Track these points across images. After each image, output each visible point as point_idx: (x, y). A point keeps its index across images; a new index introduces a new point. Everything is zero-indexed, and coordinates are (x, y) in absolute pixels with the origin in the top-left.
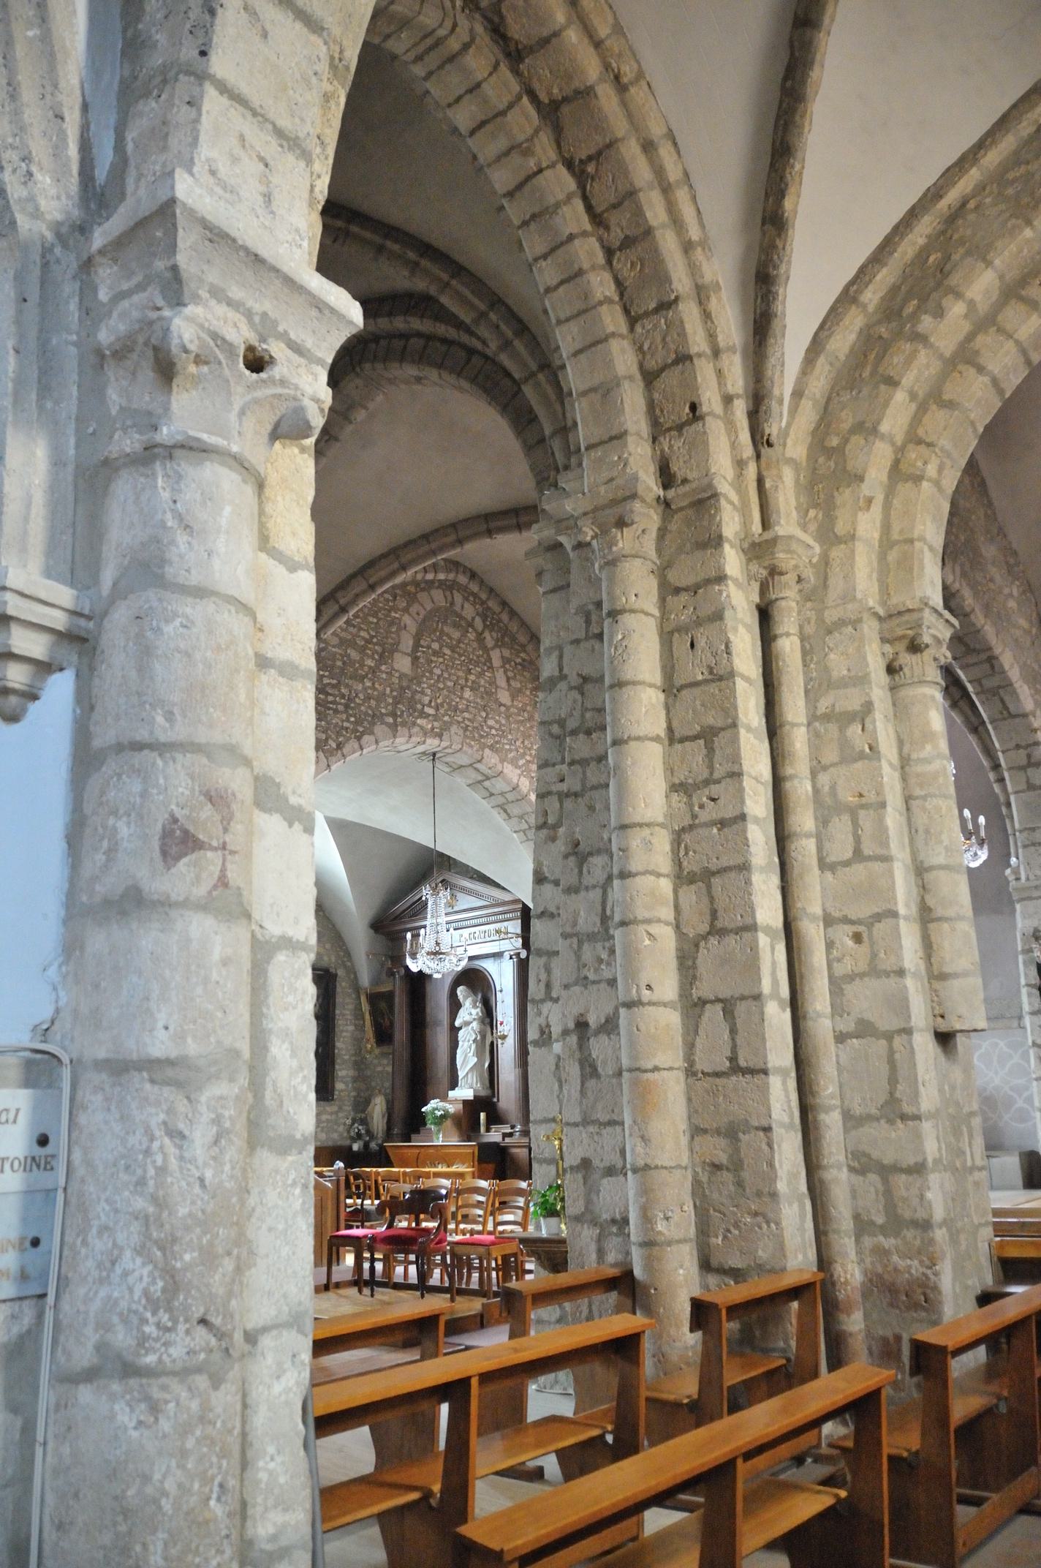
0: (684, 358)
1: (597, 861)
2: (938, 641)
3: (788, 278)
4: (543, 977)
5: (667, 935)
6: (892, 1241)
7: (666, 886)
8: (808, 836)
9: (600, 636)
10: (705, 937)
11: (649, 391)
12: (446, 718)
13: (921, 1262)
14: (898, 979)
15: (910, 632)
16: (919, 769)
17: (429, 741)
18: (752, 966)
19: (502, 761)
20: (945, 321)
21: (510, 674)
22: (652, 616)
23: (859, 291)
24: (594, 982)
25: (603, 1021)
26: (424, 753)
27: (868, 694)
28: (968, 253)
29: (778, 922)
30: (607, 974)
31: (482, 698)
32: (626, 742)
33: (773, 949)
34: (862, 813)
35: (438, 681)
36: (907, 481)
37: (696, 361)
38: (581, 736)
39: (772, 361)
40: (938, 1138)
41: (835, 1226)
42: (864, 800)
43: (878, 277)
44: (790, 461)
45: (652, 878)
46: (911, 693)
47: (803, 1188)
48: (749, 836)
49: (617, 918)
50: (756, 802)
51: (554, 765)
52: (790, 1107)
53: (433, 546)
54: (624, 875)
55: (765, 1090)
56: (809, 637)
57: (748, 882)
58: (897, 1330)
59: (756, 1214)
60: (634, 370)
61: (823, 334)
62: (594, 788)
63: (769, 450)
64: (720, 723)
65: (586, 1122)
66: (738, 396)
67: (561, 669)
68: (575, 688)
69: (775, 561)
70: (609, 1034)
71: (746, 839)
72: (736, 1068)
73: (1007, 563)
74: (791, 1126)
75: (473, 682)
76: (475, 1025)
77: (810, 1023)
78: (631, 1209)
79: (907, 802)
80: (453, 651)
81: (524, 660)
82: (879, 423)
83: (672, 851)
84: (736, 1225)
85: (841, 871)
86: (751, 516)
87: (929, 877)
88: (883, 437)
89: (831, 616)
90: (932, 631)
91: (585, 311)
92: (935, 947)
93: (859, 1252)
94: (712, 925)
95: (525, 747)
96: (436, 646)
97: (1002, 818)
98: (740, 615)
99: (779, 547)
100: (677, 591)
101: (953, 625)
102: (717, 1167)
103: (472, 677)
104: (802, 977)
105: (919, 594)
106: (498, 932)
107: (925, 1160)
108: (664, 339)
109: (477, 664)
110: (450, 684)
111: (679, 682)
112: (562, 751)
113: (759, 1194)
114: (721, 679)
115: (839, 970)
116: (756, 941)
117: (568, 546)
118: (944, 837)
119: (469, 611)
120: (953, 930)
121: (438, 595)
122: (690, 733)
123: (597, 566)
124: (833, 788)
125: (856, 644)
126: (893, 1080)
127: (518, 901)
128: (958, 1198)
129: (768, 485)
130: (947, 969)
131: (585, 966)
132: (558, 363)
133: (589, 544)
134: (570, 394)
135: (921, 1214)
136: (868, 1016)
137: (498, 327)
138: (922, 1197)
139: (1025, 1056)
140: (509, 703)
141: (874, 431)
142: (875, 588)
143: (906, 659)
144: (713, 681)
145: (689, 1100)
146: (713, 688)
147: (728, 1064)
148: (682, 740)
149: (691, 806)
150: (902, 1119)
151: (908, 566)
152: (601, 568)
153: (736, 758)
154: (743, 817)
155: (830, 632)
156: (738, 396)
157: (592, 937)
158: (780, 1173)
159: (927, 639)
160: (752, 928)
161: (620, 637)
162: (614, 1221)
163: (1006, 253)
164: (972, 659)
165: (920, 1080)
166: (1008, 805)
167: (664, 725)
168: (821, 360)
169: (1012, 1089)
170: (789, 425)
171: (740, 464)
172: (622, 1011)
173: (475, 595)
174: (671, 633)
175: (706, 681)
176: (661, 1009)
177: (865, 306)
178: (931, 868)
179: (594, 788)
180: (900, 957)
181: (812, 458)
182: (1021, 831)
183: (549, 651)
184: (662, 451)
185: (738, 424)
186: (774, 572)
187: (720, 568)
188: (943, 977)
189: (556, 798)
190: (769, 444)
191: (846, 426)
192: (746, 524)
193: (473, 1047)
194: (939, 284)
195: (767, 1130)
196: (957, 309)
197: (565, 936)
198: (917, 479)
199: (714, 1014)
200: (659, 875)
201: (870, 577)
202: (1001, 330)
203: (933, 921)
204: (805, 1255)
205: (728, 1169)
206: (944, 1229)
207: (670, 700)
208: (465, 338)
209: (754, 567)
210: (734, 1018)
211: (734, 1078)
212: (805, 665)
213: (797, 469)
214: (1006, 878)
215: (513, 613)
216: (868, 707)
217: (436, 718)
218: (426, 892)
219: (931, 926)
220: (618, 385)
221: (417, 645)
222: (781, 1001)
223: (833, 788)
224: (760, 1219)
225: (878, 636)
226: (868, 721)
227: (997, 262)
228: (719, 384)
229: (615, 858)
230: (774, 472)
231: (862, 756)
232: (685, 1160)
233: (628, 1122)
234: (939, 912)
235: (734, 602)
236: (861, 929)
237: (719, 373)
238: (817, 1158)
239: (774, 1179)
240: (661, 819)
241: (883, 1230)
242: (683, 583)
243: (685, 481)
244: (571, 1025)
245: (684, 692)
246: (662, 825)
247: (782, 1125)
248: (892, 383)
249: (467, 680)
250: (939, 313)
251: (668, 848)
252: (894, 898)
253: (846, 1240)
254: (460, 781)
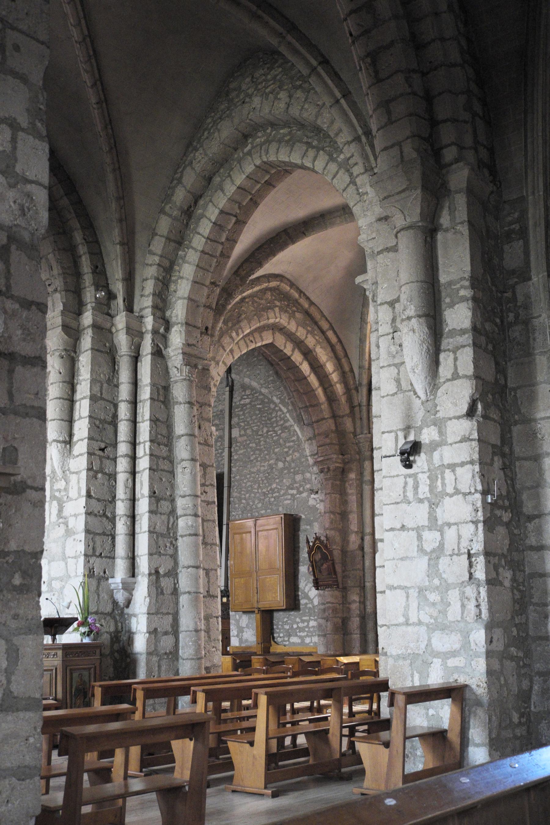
24: (163, 555)
162: (166, 653)
244: (153, 571)
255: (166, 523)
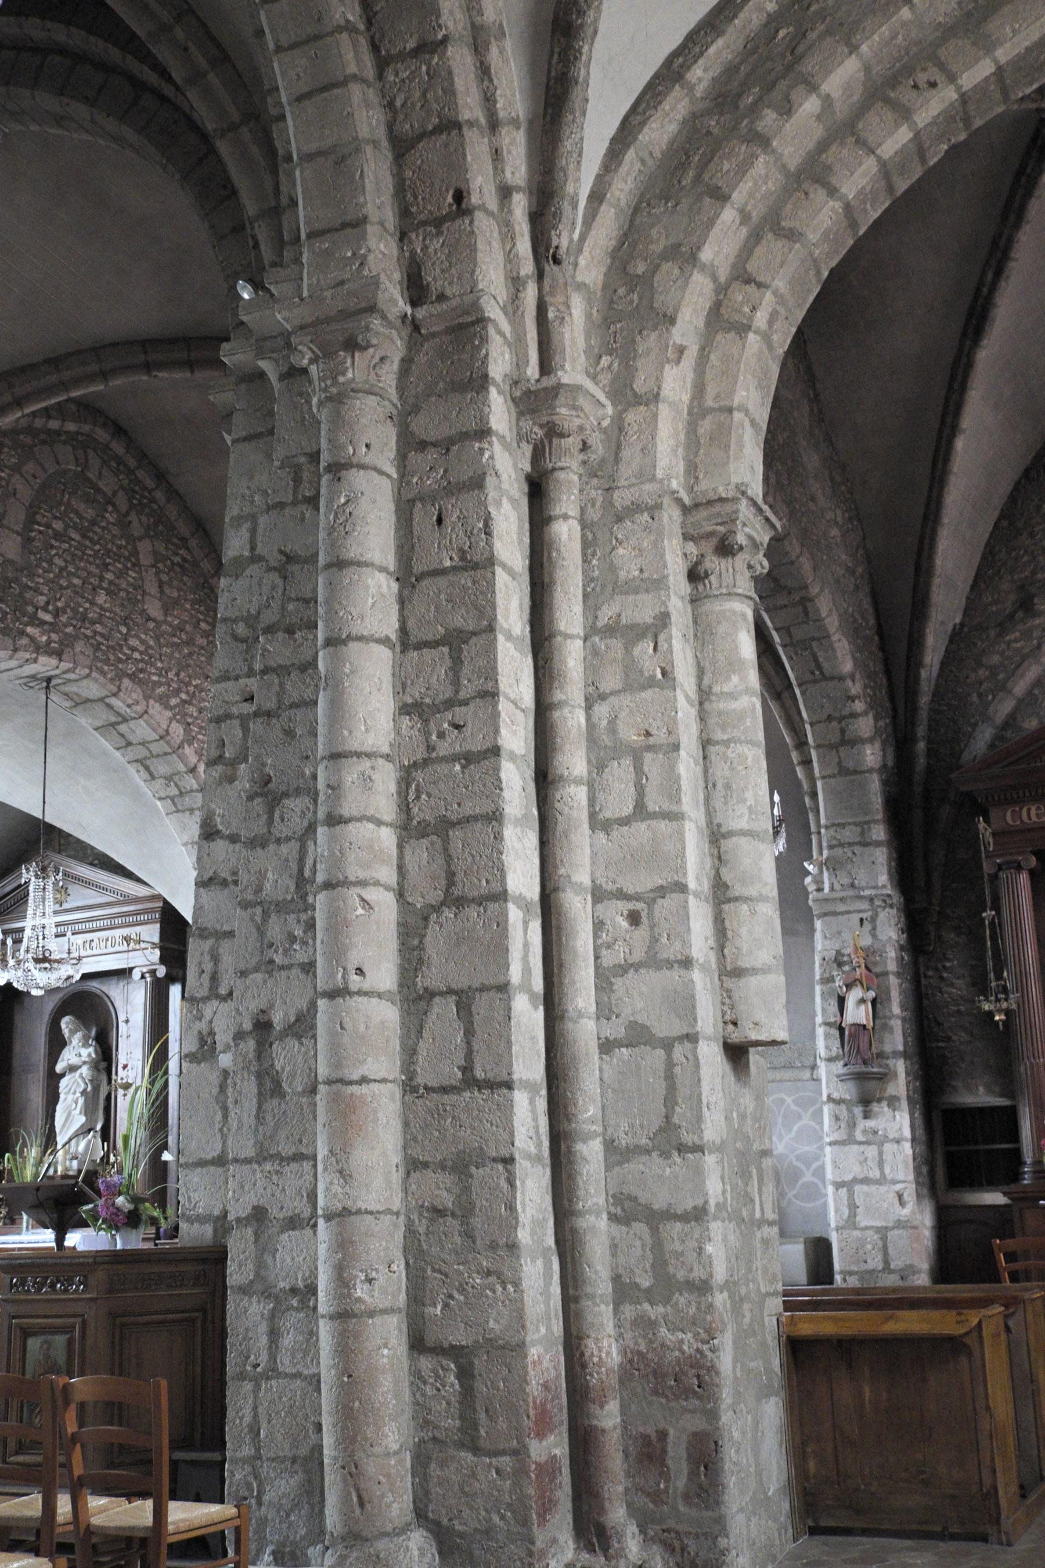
0: (451, 126)
1: (295, 805)
2: (755, 545)
3: (596, 32)
4: (208, 967)
5: (385, 903)
6: (661, 1309)
7: (388, 838)
8: (578, 782)
9: (313, 501)
10: (437, 909)
11: (400, 166)
12: (69, 630)
13: (696, 1335)
14: (683, 972)
15: (721, 529)
16: (722, 705)
17: (43, 659)
18: (499, 948)
19: (147, 698)
20: (793, 120)
21: (165, 578)
22: (388, 476)
23: (687, 67)
24: (282, 968)
25: (292, 1019)
26: (33, 677)
27: (664, 603)
28: (828, 32)
29: (533, 893)
30: (301, 955)
31: (122, 605)
32: (344, 642)
33: (526, 924)
34: (648, 757)
35: (59, 576)
36: (729, 331)
37: (465, 129)
38: (280, 635)
39: (568, 145)
40: (722, 1178)
41: (589, 1290)
42: (651, 741)
43: (712, 50)
44: (581, 287)
45: (371, 826)
46: (717, 607)
47: (550, 1241)
48: (503, 775)
49: (320, 878)
50: (515, 733)
51: (237, 678)
52: (537, 1132)
53: (66, 375)
54: (335, 820)
55: (508, 1107)
56: (593, 524)
57: (498, 837)
58: (662, 1425)
59: (489, 1273)
60: (381, 133)
61: (636, 120)
62: (294, 706)
63: (555, 268)
64: (471, 627)
65: (262, 1157)
66: (518, 189)
67: (253, 549)
68: (275, 569)
69: (555, 418)
70: (299, 1037)
71: (499, 780)
72: (470, 1081)
73: (832, 479)
74: (538, 1158)
75: (111, 583)
76: (85, 1070)
77: (570, 1025)
78: (321, 1269)
79: (704, 748)
80: (84, 536)
81: (184, 560)
82: (699, 248)
83: (399, 793)
84: (462, 1290)
85: (616, 832)
86: (526, 355)
87: (727, 844)
88: (703, 268)
89: (622, 498)
90: (747, 530)
91: (317, 37)
92: (730, 934)
93: (618, 1326)
94: (447, 892)
95: (180, 681)
96: (58, 525)
97: (803, 812)
98: (505, 486)
99: (561, 399)
100: (423, 445)
101: (773, 526)
102: (438, 1212)
103: (109, 576)
104: (561, 966)
105: (735, 479)
106: (127, 939)
107: (706, 1202)
108: (424, 94)
109: (118, 557)
110: (76, 581)
111: (418, 568)
112: (248, 661)
113: (493, 1246)
114: (475, 566)
115: (609, 959)
116: (505, 914)
117: (273, 377)
118: (749, 795)
119: (108, 484)
120: (753, 913)
121: (65, 452)
122: (430, 637)
123: (315, 401)
124: (613, 722)
125: (653, 538)
126: (670, 1100)
127: (158, 897)
128: (743, 1256)
129: (551, 315)
130: (745, 963)
131: (271, 945)
132: (274, 112)
133: (304, 371)
134: (289, 158)
135: (698, 1273)
136: (641, 1019)
137: (186, 49)
138: (700, 1250)
139: (818, 1115)
140: (161, 618)
141: (692, 258)
142: (681, 467)
143: (712, 562)
144: (464, 569)
145: (406, 1124)
146: (465, 579)
147: (459, 1075)
148: (419, 646)
149: (427, 734)
150: (679, 1151)
151: (721, 437)
152: (321, 403)
153: (490, 672)
154: (495, 751)
155: (619, 519)
156: (518, 189)
157: (282, 907)
158: (522, 1218)
159: (741, 539)
160: (501, 896)
161: (343, 500)
162: (294, 1291)
163: (876, 37)
164: (782, 600)
165: (705, 1101)
166: (814, 795)
167: (396, 625)
168: (630, 155)
169: (798, 1158)
170: (583, 238)
171: (516, 283)
172: (322, 1003)
173: (119, 461)
174: (412, 502)
175: (454, 569)
176: (375, 1001)
177: (691, 88)
178: (730, 834)
179: (294, 706)
180: (686, 943)
181: (608, 286)
182: (827, 827)
183: (239, 520)
184: (413, 253)
185: (517, 228)
186: (553, 432)
187: (484, 419)
188: (738, 973)
189: (236, 723)
190: (557, 261)
191: (657, 248)
192: (520, 363)
193: (81, 1101)
194: (789, 68)
195: (508, 1161)
196: (811, 105)
197: (245, 905)
198: (743, 329)
199: (445, 1009)
200: (379, 823)
201: (674, 452)
202: (861, 143)
203: (729, 900)
204: (549, 1328)
205: (453, 1215)
206: (726, 1294)
207: (406, 592)
208: (134, 66)
209: (527, 424)
210: (471, 1014)
211: (467, 1094)
212: (585, 561)
213: (589, 301)
214: (805, 889)
215: (173, 494)
216: (664, 619)
217: (53, 627)
218: (28, 874)
219: (726, 907)
220: (358, 150)
221: (30, 521)
222: (532, 996)
223: (613, 722)
224: (492, 1279)
225: (680, 531)
226: (661, 638)
227: (864, 48)
228: (495, 168)
229: (322, 798)
230: (560, 299)
231: (651, 683)
232: (397, 1204)
233: (322, 1152)
234: (737, 890)
235: (499, 466)
236: (639, 906)
237: (497, 154)
238: (570, 1201)
239: (513, 1223)
240: (386, 749)
241: (649, 1295)
242: (433, 435)
243: (442, 297)
244: (247, 1026)
245: (425, 582)
246: (387, 757)
247: (528, 1156)
248: (721, 197)
249: (102, 578)
250: (787, 110)
251: (393, 788)
252: (683, 867)
253: (603, 1307)
254: (84, 721)
255: (294, 866)
